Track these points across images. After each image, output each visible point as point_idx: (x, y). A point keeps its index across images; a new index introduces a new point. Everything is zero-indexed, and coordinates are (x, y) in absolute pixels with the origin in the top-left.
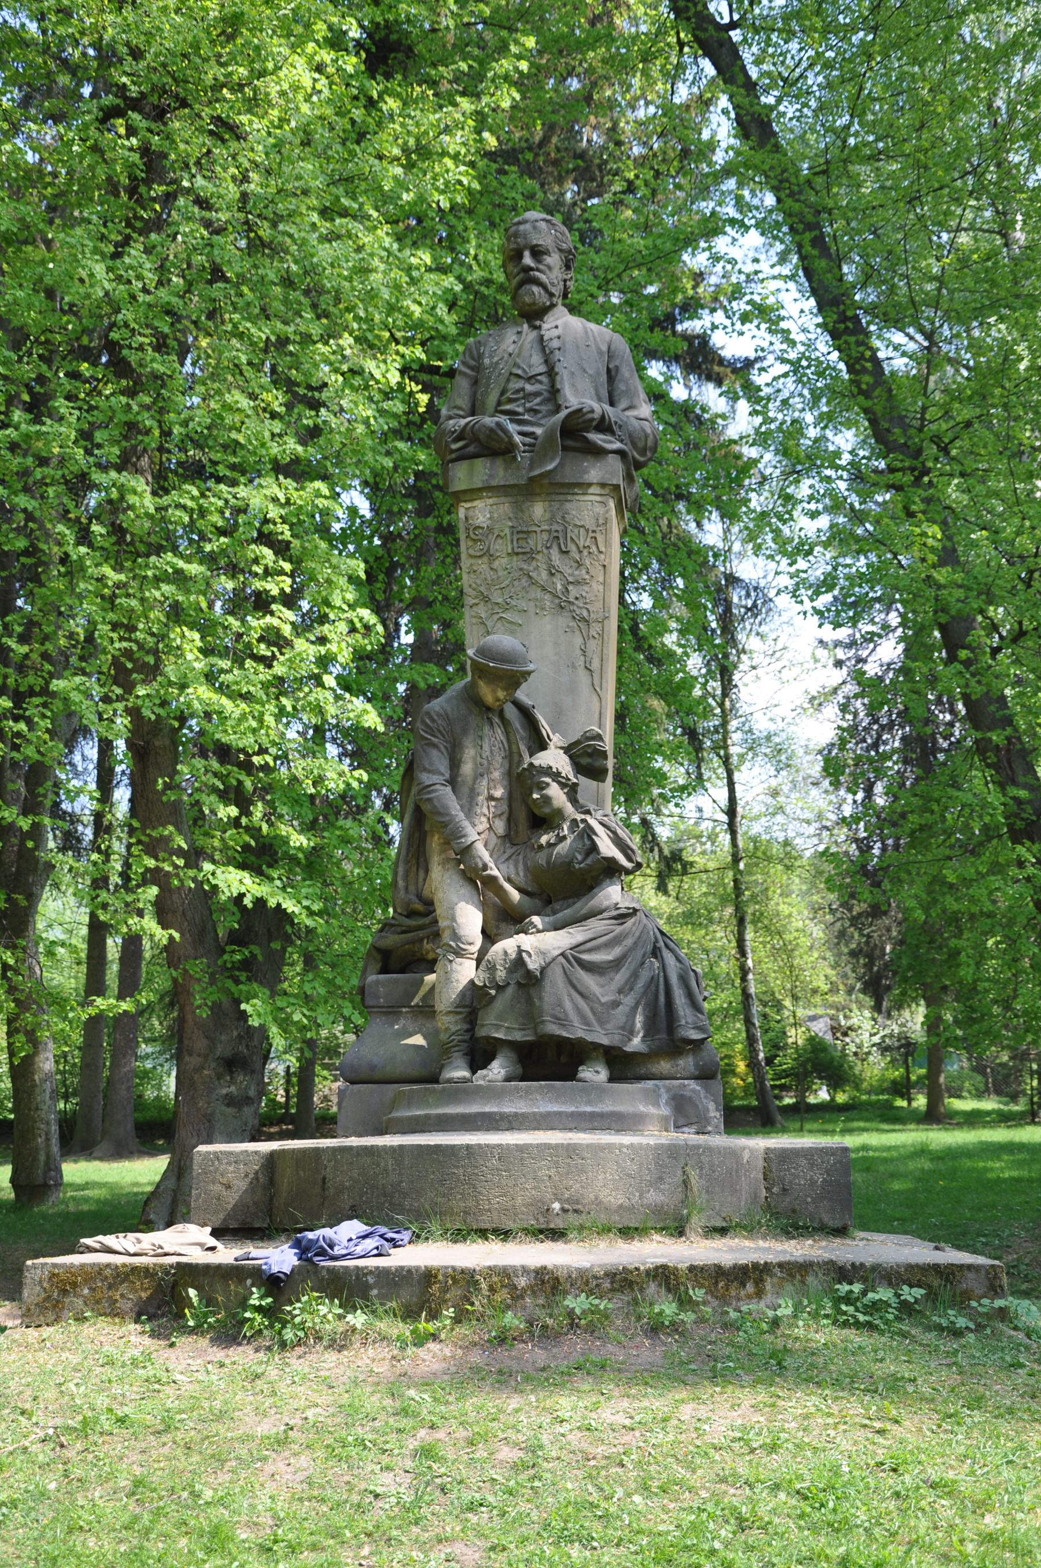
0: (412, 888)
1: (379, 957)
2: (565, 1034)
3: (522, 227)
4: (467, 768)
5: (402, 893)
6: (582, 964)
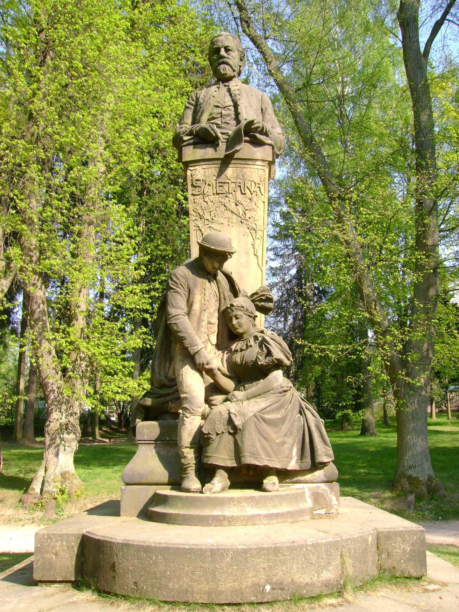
0: (162, 373)
1: (143, 411)
2: (257, 463)
3: (220, 38)
4: (196, 306)
5: (157, 375)
6: (264, 420)
